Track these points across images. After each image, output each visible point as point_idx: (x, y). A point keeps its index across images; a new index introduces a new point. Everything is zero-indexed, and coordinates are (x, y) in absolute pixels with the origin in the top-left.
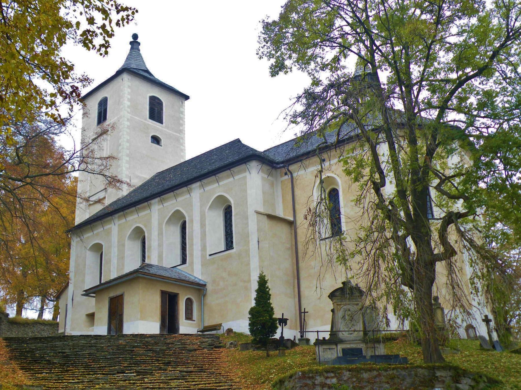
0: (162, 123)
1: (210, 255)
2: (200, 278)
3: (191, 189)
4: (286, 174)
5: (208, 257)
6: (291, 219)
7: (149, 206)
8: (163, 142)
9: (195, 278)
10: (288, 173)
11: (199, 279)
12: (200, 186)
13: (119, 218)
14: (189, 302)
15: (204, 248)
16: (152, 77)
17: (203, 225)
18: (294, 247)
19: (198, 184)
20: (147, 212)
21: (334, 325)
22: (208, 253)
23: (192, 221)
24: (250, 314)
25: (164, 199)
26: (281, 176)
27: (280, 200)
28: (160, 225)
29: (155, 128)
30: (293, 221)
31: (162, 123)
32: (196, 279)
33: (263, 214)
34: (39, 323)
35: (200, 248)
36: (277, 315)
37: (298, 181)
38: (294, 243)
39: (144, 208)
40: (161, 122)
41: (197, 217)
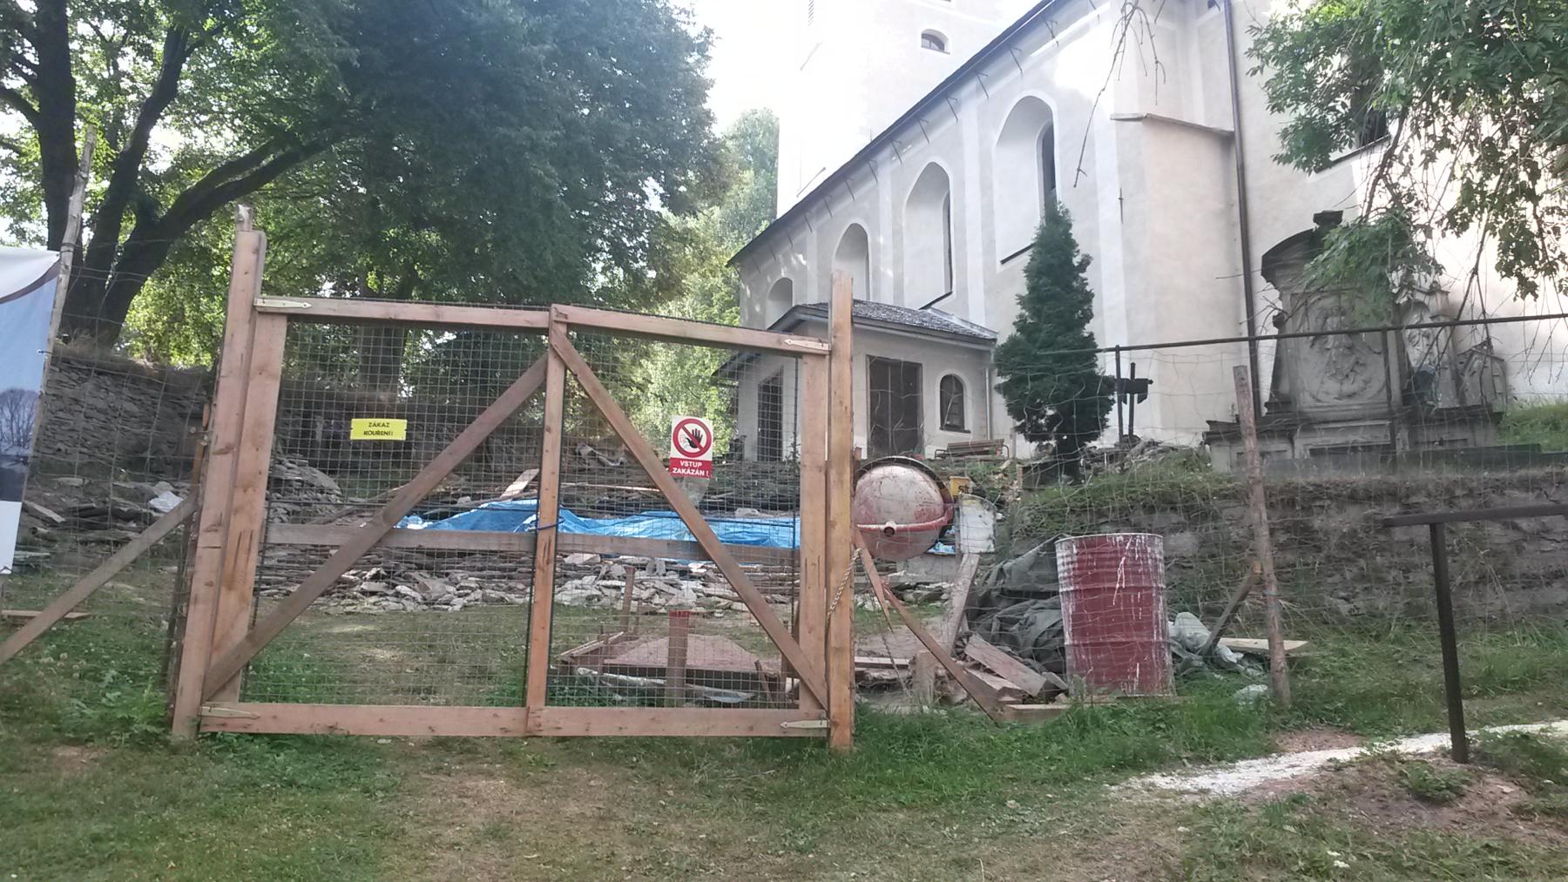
1: (1003, 262)
3: (959, 104)
5: (999, 268)
6: (1229, 126)
7: (873, 172)
8: (949, 46)
9: (973, 325)
11: (983, 329)
12: (977, 90)
13: (819, 213)
14: (951, 386)
15: (989, 245)
18: (1236, 209)
20: (871, 184)
21: (1285, 369)
23: (962, 183)
24: (708, 113)
25: (903, 146)
26: (1199, 14)
27: (1197, 83)
28: (896, 208)
30: (1232, 134)
33: (1138, 119)
34: (168, 41)
35: (980, 250)
38: (1236, 198)
39: (864, 180)
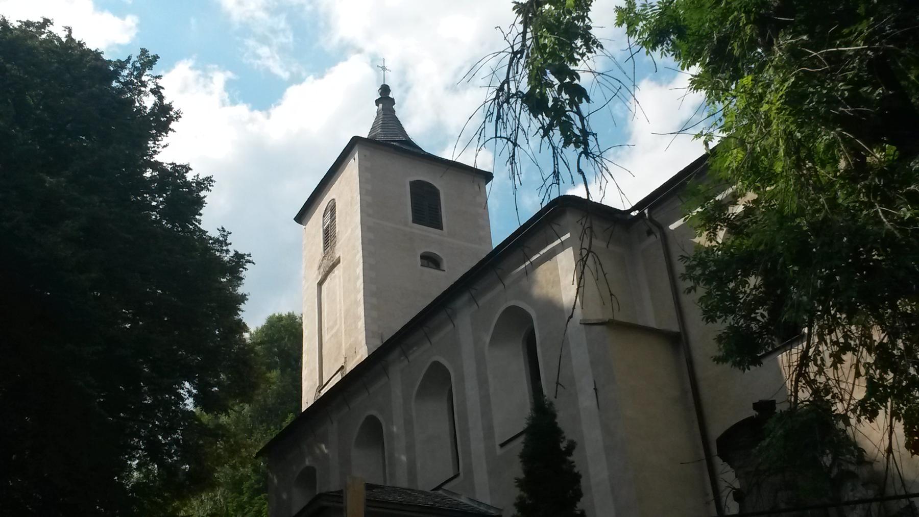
0: (442, 229)
1: (502, 445)
2: (489, 503)
4: (650, 233)
6: (675, 328)
8: (445, 265)
9: (480, 503)
10: (655, 229)
16: (416, 150)
17: (483, 382)
19: (465, 298)
22: (499, 440)
29: (428, 238)
31: (442, 229)
32: (482, 508)
36: (201, 212)
37: (407, 88)
38: (688, 386)
40: (439, 226)
41: (469, 367)
